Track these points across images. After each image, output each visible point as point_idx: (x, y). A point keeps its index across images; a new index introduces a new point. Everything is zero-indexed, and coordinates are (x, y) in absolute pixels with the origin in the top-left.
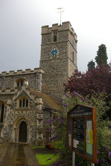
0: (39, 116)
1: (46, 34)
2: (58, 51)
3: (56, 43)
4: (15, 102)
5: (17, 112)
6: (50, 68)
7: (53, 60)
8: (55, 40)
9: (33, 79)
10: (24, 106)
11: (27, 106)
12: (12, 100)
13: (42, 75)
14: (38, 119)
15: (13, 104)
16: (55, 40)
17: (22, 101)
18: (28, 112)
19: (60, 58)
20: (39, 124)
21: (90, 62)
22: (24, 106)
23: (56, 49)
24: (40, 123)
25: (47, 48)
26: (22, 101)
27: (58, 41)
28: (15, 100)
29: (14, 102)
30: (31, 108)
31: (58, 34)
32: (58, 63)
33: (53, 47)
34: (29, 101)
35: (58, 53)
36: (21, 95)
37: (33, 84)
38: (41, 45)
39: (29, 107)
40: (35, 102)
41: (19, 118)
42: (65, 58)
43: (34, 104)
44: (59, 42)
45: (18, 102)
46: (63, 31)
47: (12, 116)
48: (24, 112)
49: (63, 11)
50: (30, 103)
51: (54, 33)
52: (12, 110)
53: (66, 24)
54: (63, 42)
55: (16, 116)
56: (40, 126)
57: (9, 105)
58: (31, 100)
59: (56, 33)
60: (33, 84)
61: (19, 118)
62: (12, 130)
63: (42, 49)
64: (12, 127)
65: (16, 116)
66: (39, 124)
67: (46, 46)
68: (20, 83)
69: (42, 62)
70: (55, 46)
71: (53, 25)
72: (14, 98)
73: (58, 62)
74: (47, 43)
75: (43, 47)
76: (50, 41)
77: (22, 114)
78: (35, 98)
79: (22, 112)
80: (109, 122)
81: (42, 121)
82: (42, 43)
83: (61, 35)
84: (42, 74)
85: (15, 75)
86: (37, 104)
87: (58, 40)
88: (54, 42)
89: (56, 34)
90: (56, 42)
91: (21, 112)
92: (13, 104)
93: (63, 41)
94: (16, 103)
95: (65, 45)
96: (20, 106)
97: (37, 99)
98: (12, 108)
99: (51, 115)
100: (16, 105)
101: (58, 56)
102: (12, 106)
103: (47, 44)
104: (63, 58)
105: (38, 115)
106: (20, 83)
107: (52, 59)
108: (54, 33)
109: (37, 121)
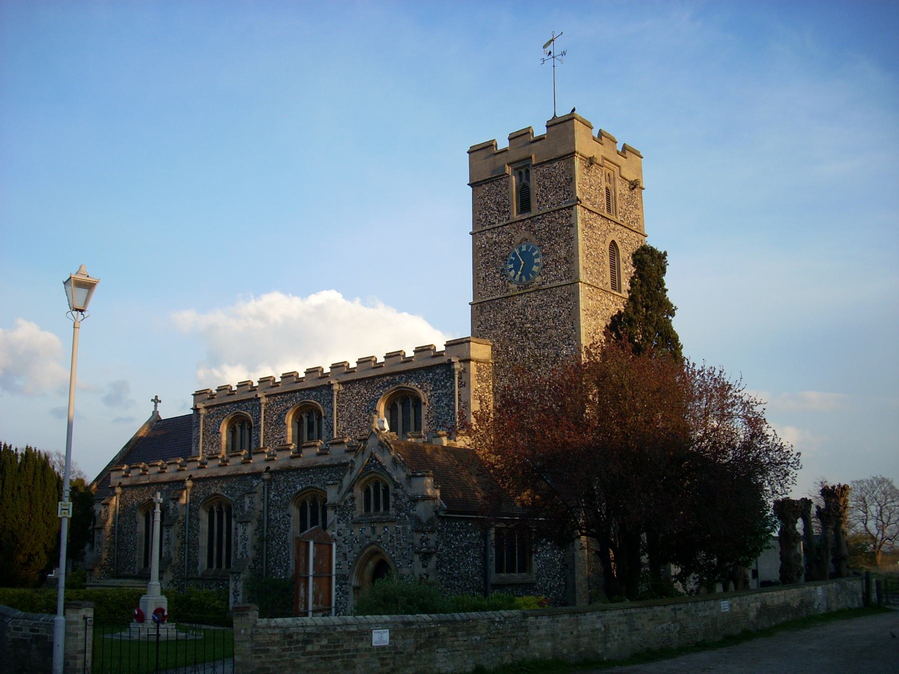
0: (422, 541)
1: (486, 182)
2: (537, 256)
3: (529, 218)
4: (350, 494)
5: (356, 532)
6: (511, 330)
7: (522, 294)
8: (525, 205)
9: (442, 386)
10: (377, 508)
11: (387, 508)
12: (340, 488)
13: (479, 370)
14: (418, 553)
15: (346, 502)
16: (525, 205)
17: (372, 489)
18: (391, 528)
19: (548, 285)
20: (424, 570)
21: (666, 287)
22: (377, 508)
23: (528, 248)
24: (424, 566)
25: (495, 243)
26: (372, 489)
27: (534, 212)
28: (351, 489)
29: (347, 497)
30: (398, 515)
31: (534, 175)
32: (541, 307)
33: (518, 240)
34: (391, 487)
35: (537, 264)
36: (366, 468)
37: (446, 409)
38: (471, 234)
39: (392, 511)
40: (411, 492)
41: (366, 552)
42: (564, 282)
43: (406, 499)
44: (537, 213)
45: (359, 492)
46: (551, 161)
47: (343, 545)
48: (379, 529)
49: (564, 54)
50: (396, 495)
51: (517, 172)
52: (342, 525)
53: (561, 126)
54: (554, 211)
55: (356, 546)
56: (428, 576)
57: (334, 507)
58: (397, 486)
59: (527, 172)
60: (446, 409)
61: (366, 552)
62: (347, 593)
63: (476, 250)
64: (345, 584)
65: (356, 546)
66: (424, 570)
67: (489, 235)
68: (400, 408)
69: (478, 308)
70: (526, 235)
71: (510, 139)
72: (347, 480)
73: (538, 302)
74: (493, 220)
75: (478, 243)
76: (504, 212)
77: (374, 538)
78: (409, 478)
79: (373, 528)
80: (8, 635)
81: (434, 559)
82: (476, 221)
83: (547, 183)
84: (477, 361)
85: (379, 376)
86: (415, 500)
87: (534, 204)
88: (519, 217)
89: (528, 179)
90: (526, 216)
91: (370, 528)
92: (346, 502)
93: (554, 208)
94: (353, 499)
95: (562, 225)
96: (367, 509)
97: (415, 482)
98: (342, 517)
99: (485, 536)
100: (353, 507)
101: (538, 279)
102: (342, 509)
103: (494, 228)
104: (558, 283)
105: (418, 537)
106: (400, 408)
107: (518, 292)
108: (520, 173)
109: (417, 558)
